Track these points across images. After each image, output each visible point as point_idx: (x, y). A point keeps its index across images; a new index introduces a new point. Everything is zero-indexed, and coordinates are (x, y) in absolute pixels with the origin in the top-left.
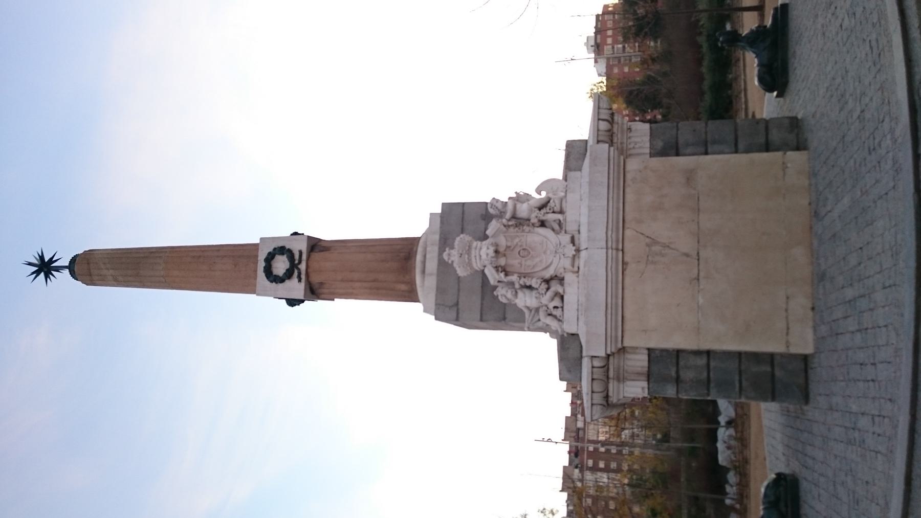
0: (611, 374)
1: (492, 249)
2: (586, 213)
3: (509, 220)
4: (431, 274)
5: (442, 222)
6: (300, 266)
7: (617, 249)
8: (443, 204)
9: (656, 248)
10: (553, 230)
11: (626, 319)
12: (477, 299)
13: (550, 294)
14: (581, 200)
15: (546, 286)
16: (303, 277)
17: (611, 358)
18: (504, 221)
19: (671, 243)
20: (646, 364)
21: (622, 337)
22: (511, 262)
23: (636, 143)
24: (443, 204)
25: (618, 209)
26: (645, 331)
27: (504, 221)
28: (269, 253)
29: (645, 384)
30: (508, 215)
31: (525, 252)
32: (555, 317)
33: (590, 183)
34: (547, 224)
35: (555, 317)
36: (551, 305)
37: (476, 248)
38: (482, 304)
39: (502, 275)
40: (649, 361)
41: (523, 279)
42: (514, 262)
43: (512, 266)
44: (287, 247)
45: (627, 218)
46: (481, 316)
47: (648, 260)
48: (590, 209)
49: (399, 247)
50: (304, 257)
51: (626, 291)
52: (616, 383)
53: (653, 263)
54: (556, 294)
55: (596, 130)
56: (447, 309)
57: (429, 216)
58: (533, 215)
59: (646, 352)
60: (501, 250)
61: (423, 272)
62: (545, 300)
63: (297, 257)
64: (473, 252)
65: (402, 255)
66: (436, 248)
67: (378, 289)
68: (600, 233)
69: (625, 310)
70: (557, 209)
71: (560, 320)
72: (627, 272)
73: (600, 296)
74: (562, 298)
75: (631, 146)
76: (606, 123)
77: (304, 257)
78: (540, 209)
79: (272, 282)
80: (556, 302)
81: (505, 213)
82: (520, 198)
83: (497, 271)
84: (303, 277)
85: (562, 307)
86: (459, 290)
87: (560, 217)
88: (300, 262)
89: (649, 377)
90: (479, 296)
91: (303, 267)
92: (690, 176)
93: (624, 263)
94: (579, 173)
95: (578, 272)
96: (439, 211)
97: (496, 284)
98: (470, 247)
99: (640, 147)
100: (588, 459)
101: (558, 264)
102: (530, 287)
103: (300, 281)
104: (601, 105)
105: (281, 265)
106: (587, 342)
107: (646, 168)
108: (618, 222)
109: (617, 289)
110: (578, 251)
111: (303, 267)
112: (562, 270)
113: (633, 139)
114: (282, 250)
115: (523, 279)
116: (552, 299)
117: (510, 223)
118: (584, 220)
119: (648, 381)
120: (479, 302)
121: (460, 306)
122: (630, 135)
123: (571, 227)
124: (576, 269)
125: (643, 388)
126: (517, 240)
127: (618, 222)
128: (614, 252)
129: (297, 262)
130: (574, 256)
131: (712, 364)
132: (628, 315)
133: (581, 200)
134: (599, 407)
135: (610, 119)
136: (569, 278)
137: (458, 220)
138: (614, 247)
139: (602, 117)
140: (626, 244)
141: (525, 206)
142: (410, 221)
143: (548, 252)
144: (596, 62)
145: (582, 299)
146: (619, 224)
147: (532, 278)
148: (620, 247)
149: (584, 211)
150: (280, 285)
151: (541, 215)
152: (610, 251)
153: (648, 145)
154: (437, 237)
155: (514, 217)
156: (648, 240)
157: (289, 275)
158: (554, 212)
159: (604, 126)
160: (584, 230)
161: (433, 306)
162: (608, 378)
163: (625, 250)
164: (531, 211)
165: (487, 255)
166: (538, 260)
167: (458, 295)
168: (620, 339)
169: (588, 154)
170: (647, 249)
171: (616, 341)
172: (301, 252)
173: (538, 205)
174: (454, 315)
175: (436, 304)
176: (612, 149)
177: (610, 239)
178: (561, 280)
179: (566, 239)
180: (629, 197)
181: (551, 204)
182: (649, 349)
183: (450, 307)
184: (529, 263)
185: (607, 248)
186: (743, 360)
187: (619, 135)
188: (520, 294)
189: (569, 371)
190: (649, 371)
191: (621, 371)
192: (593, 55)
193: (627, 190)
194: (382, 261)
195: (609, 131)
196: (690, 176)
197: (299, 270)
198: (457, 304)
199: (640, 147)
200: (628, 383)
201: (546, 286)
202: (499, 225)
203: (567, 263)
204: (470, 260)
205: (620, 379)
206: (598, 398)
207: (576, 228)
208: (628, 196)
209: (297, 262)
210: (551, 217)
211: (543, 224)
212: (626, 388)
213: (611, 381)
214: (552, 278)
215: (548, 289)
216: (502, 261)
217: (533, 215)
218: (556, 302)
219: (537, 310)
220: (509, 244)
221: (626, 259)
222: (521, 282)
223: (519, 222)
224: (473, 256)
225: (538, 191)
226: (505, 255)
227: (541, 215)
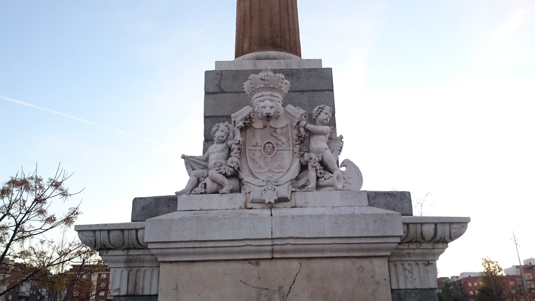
0: (133, 252)
1: (272, 112)
2: (316, 214)
4: (255, 65)
5: (310, 70)
7: (273, 252)
8: (331, 69)
10: (297, 179)
11: (191, 265)
13: (220, 178)
14: (333, 207)
15: (229, 174)
20: (147, 292)
21: (171, 262)
22: (258, 134)
24: (331, 69)
25: (323, 251)
26: (177, 289)
27: (304, 123)
29: (123, 292)
30: (310, 126)
31: (270, 149)
33: (353, 215)
36: (208, 181)
37: (272, 95)
39: (241, 124)
40: (149, 295)
41: (237, 147)
42: (258, 138)
43: (254, 136)
45: (314, 262)
47: (262, 289)
48: (319, 217)
49: (287, 38)
51: (224, 264)
52: (125, 257)
53: (259, 295)
54: (221, 186)
55: (423, 222)
56: (217, 83)
57: (317, 58)
58: (312, 155)
60: (272, 123)
61: (258, 58)
62: (213, 173)
64: (268, 93)
65: (279, 40)
66: (284, 67)
68: (292, 230)
69: (201, 264)
70: (322, 182)
72: (247, 265)
73: (214, 234)
74: (217, 192)
75: (407, 266)
76: (432, 233)
78: (322, 163)
80: (211, 186)
81: (315, 124)
82: (335, 142)
83: (246, 119)
85: (206, 193)
86: (238, 92)
87: (313, 184)
93: (257, 261)
94: (367, 204)
95: (246, 208)
96: (324, 66)
97: (233, 119)
98: (273, 89)
99: (406, 277)
101: (254, 186)
102: (229, 156)
104: (454, 226)
106: (160, 221)
107: (378, 283)
108: (306, 251)
109: (225, 253)
110: (271, 206)
112: (248, 190)
113: (415, 269)
115: (237, 147)
116: (214, 181)
117: (302, 130)
118: (307, 211)
119: (127, 295)
121: (220, 95)
122: (421, 264)
123: (299, 197)
124: (249, 205)
125: (119, 290)
126: (284, 140)
127: (306, 251)
128: (270, 248)
130: (263, 202)
132: (197, 267)
133: (333, 207)
134: (92, 239)
135: (438, 238)
136: (239, 199)
137: (315, 87)
138: (275, 247)
139: (439, 227)
141: (324, 145)
142: (315, 43)
143: (270, 175)
144: (517, 267)
145: (212, 214)
146: (305, 252)
147: (239, 158)
148: (276, 256)
149: (319, 211)
151: (314, 163)
152: (269, 243)
153: (410, 286)
154: (295, 67)
155: (311, 133)
156: (287, 288)
158: (318, 178)
159: (428, 230)
160: (296, 212)
162: (128, 249)
163: (273, 262)
164: (318, 152)
165: (264, 107)
166: (261, 163)
168: (167, 259)
169: (389, 212)
170: (276, 288)
171: (163, 255)
173: (326, 160)
174: (211, 90)
177: (284, 242)
179: (284, 192)
180: (339, 264)
181: (328, 175)
182: (156, 296)
184: (258, 154)
185: (272, 239)
187: (418, 251)
188: (221, 146)
189: (144, 208)
190: (138, 296)
191: (138, 264)
192: (522, 264)
193: (348, 262)
194: (271, 22)
195: (422, 237)
198: (222, 92)
199: (406, 277)
200: (125, 273)
201: (229, 174)
202: (298, 116)
203: (255, 195)
204: (258, 90)
205: (129, 262)
207: (298, 204)
210: (312, 174)
211: (304, 167)
212: (119, 270)
213: (125, 252)
214: (240, 180)
215: (225, 175)
216: (258, 124)
217: (312, 155)
218: (211, 186)
219: (206, 167)
220: (278, 131)
221: (262, 263)
222: (233, 146)
223: (304, 139)
224: (264, 93)
225: (347, 163)
226: (265, 127)
227: (314, 163)
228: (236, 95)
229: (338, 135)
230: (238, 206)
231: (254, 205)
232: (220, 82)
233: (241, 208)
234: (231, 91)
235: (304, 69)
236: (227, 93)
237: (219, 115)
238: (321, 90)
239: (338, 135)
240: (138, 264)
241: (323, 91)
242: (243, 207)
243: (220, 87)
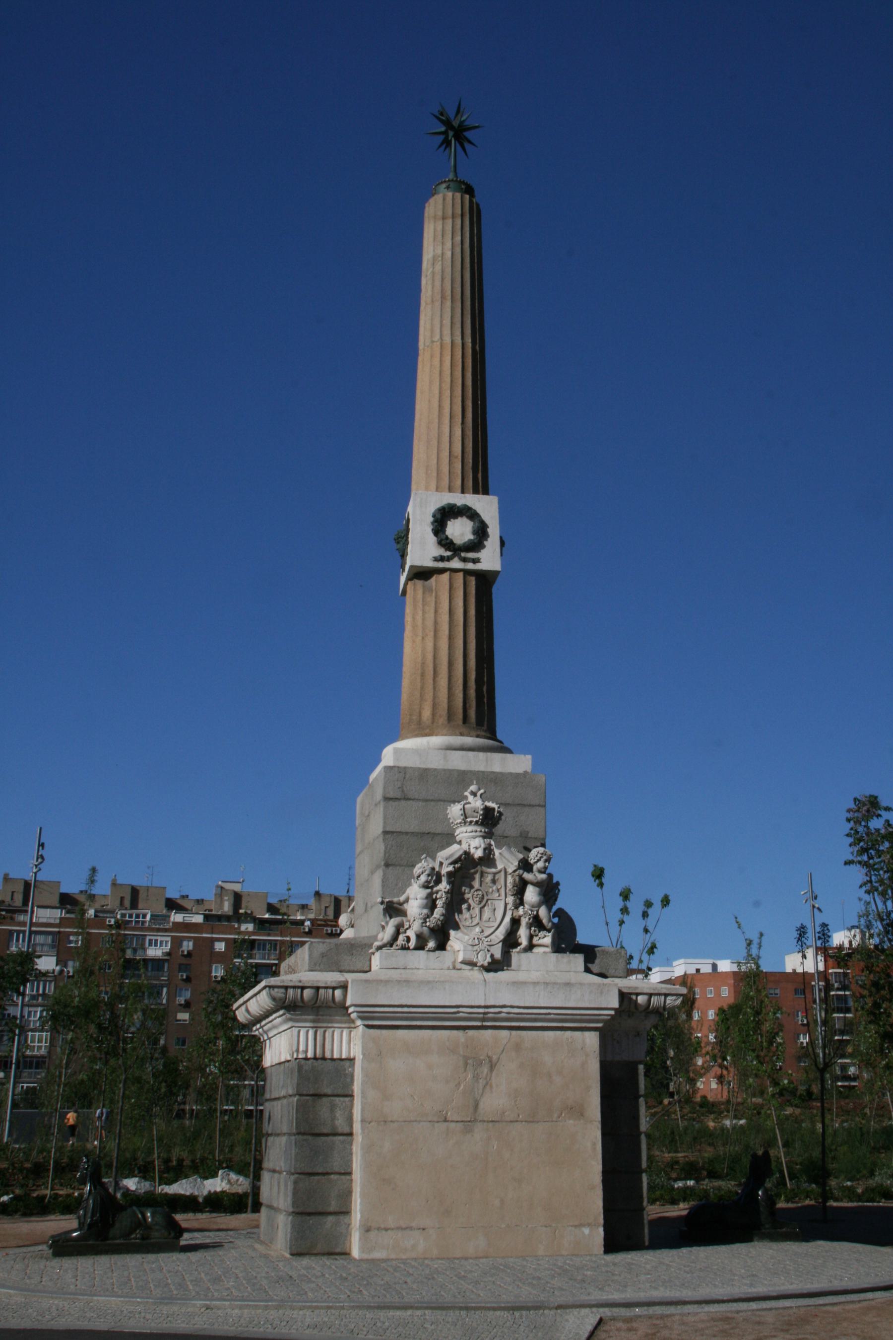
6: (456, 559)
9: (485, 1070)
12: (413, 826)
19: (491, 1086)
20: (336, 1056)
38: (407, 833)
50: (470, 566)
53: (466, 1064)
56: (399, 784)
63: (471, 555)
67: (423, 675)
84: (441, 565)
88: (465, 560)
90: (416, 830)
95: (454, 968)
100: (159, 980)
103: (436, 559)
104: (669, 998)
107: (587, 1055)
111: (456, 564)
120: (411, 830)
121: (403, 802)
140: (490, 1032)
157: (446, 543)
161: (403, 764)
172: (476, 561)
174: (391, 795)
175: (405, 768)
183: (401, 788)
191: (325, 1025)
196: (577, 1111)
197: (449, 559)
208: (551, 1034)
209: (463, 554)
228: (424, 804)
229: (554, 881)
230: (446, 966)
231: (464, 966)
232: (403, 784)
233: (449, 969)
234: (416, 797)
235: (511, 774)
236: (413, 800)
237: (403, 830)
238: (530, 805)
239: (554, 881)
240: (325, 1025)
241: (533, 806)
242: (451, 967)
243: (403, 791)
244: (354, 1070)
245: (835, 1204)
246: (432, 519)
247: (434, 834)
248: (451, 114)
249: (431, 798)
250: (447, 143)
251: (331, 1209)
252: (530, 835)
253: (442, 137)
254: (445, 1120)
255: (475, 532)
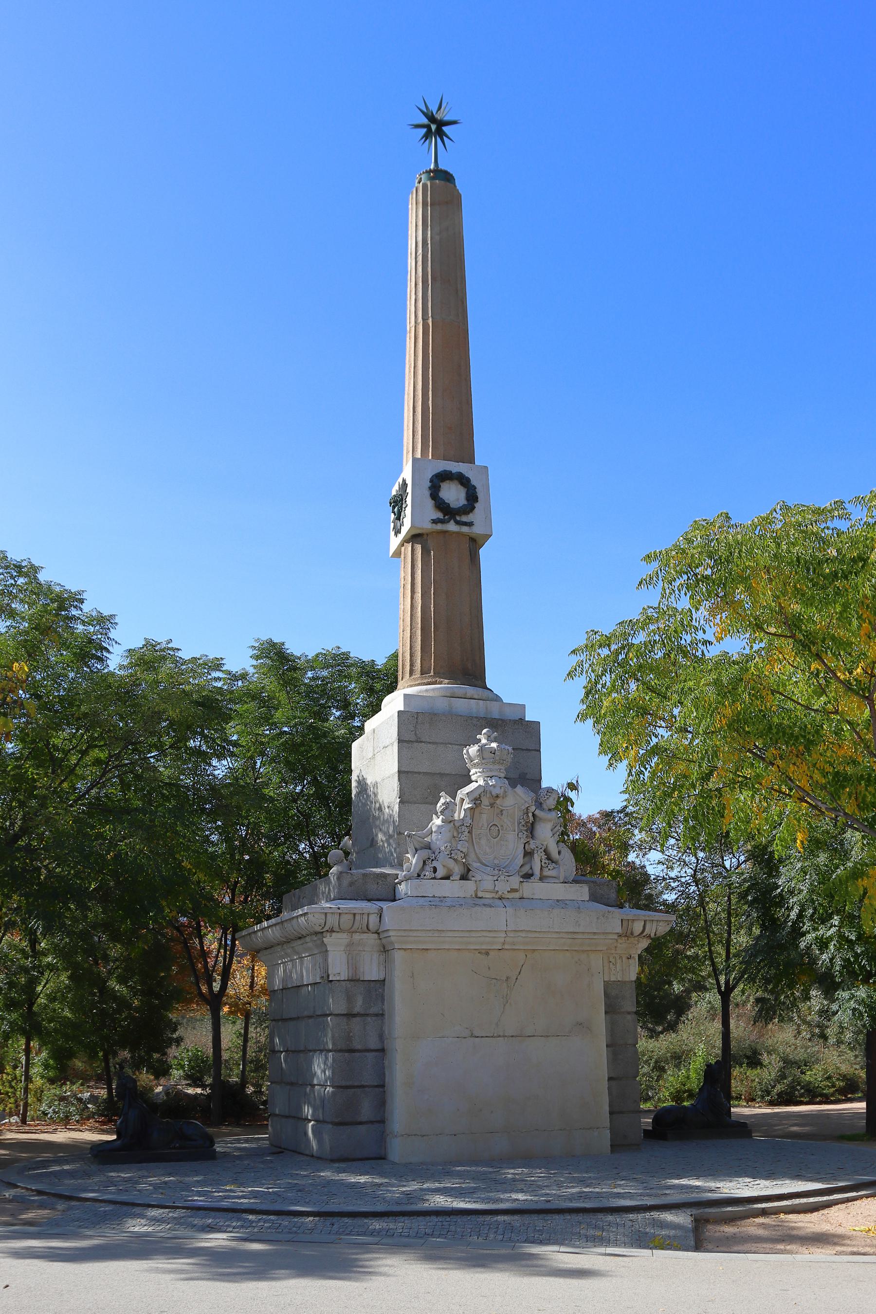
0: (357, 937)
3: (534, 815)
6: (452, 522)
16: (439, 527)
17: (376, 935)
18: (533, 808)
20: (367, 978)
23: (615, 964)
28: (468, 480)
32: (423, 869)
34: (527, 859)
35: (423, 869)
38: (419, 773)
44: (476, 505)
46: (405, 772)
59: (382, 978)
63: (464, 519)
71: (419, 876)
74: (447, 878)
77: (465, 529)
79: (431, 481)
80: (441, 873)
85: (434, 878)
88: (458, 523)
89: (354, 980)
91: (452, 527)
92: (583, 1027)
103: (435, 522)
105: (453, 494)
112: (478, 877)
114: (472, 498)
117: (530, 815)
129: (458, 518)
131: (370, 1055)
148: (506, 947)
150: (427, 493)
157: (441, 505)
167: (430, 743)
172: (470, 524)
176: (616, 937)
178: (464, 877)
186: (377, 1089)
190: (358, 980)
196: (583, 1027)
206: (332, 921)
209: (458, 518)
211: (528, 854)
216: (486, 801)
244: (384, 990)
245: (747, 1111)
246: (429, 484)
247: (444, 774)
248: (433, 108)
249: (441, 741)
250: (427, 136)
251: (364, 1118)
252: (527, 777)
253: (424, 130)
254: (472, 1036)
255: (468, 499)
